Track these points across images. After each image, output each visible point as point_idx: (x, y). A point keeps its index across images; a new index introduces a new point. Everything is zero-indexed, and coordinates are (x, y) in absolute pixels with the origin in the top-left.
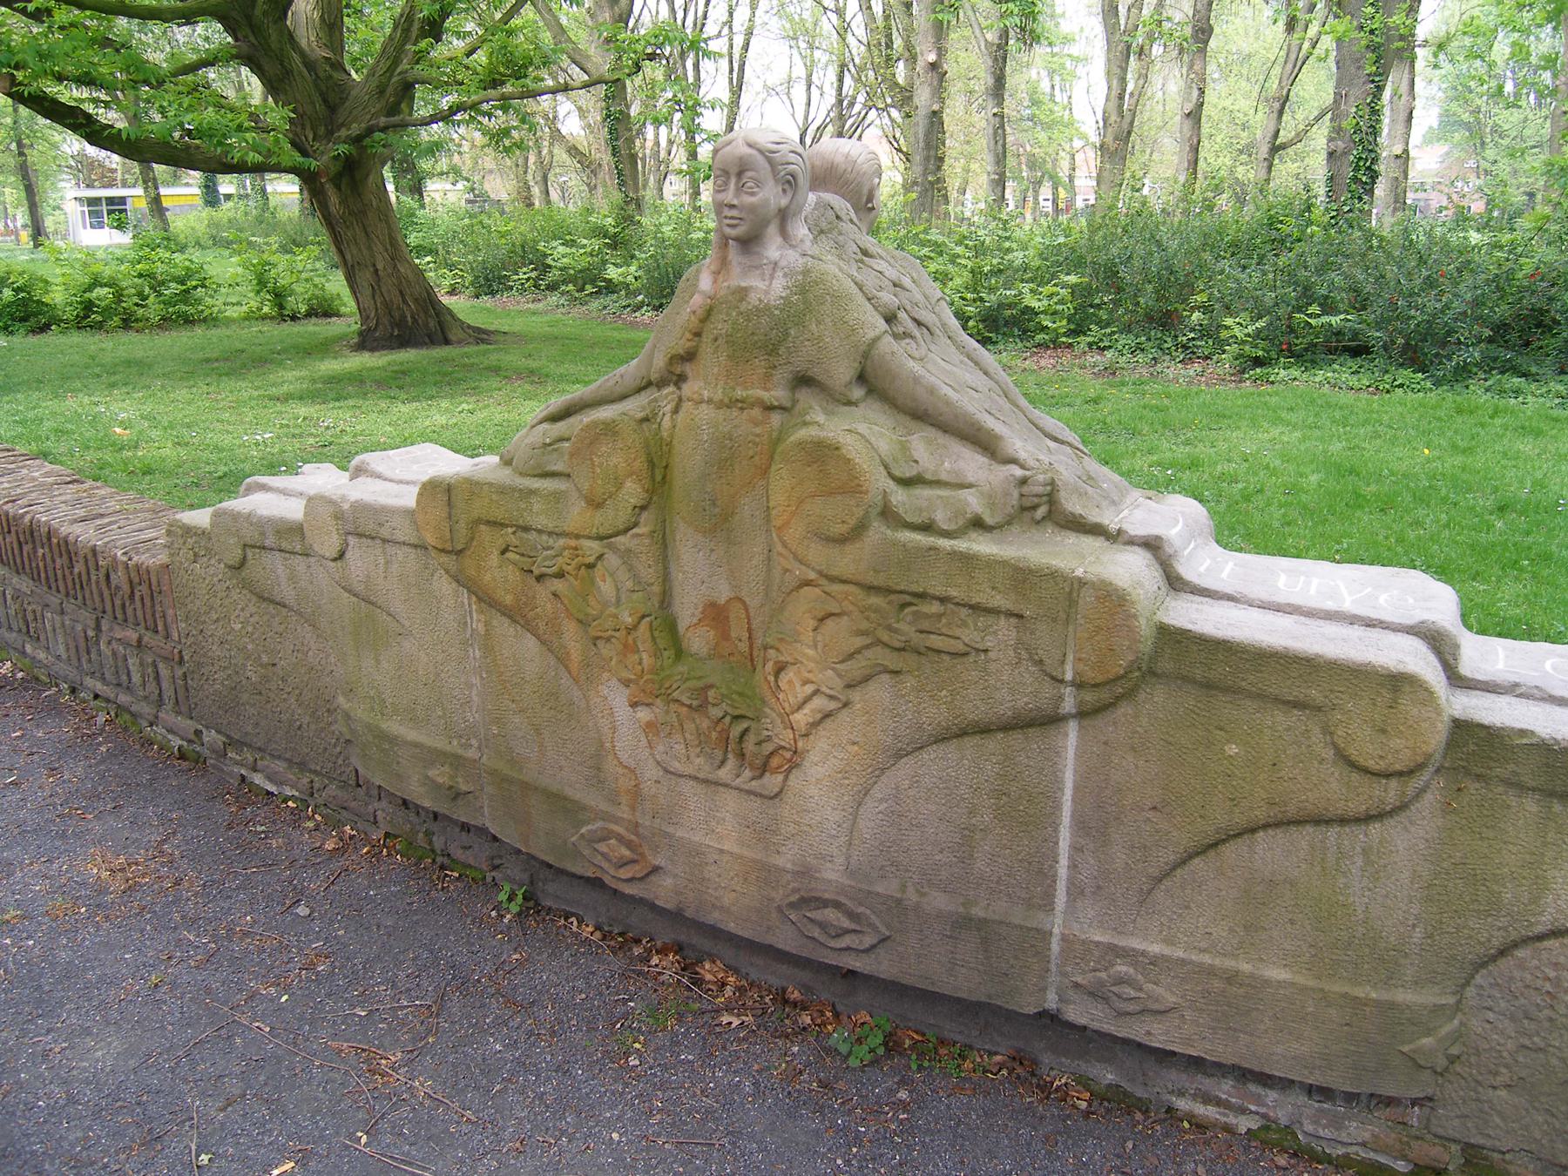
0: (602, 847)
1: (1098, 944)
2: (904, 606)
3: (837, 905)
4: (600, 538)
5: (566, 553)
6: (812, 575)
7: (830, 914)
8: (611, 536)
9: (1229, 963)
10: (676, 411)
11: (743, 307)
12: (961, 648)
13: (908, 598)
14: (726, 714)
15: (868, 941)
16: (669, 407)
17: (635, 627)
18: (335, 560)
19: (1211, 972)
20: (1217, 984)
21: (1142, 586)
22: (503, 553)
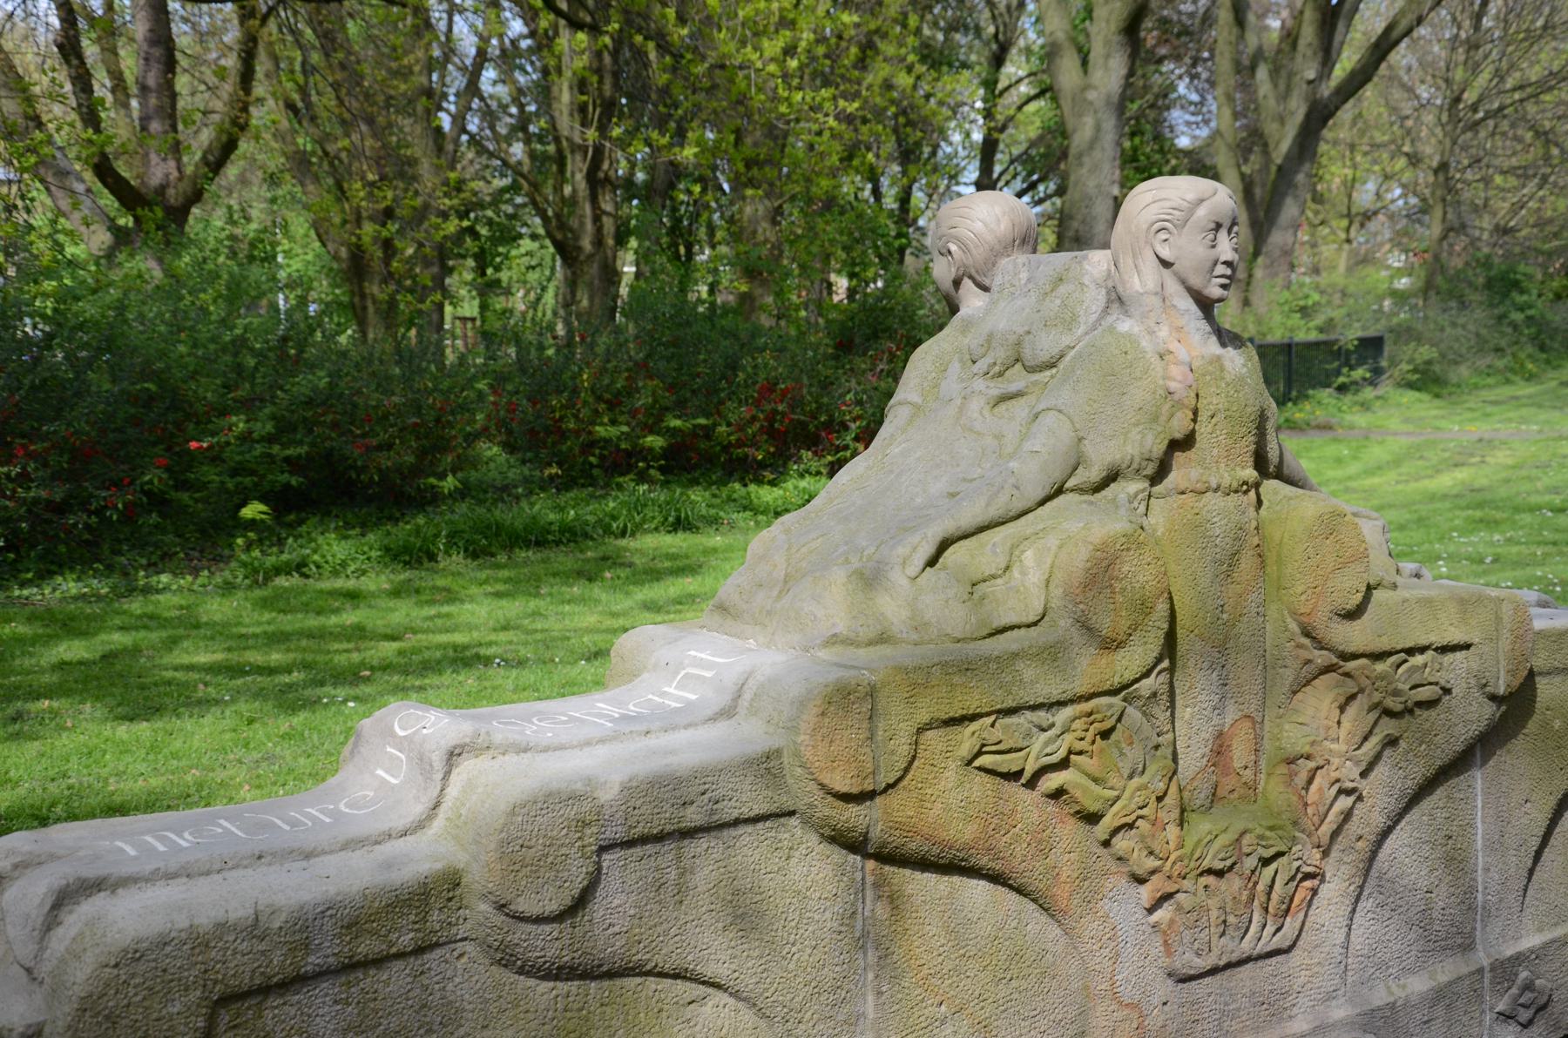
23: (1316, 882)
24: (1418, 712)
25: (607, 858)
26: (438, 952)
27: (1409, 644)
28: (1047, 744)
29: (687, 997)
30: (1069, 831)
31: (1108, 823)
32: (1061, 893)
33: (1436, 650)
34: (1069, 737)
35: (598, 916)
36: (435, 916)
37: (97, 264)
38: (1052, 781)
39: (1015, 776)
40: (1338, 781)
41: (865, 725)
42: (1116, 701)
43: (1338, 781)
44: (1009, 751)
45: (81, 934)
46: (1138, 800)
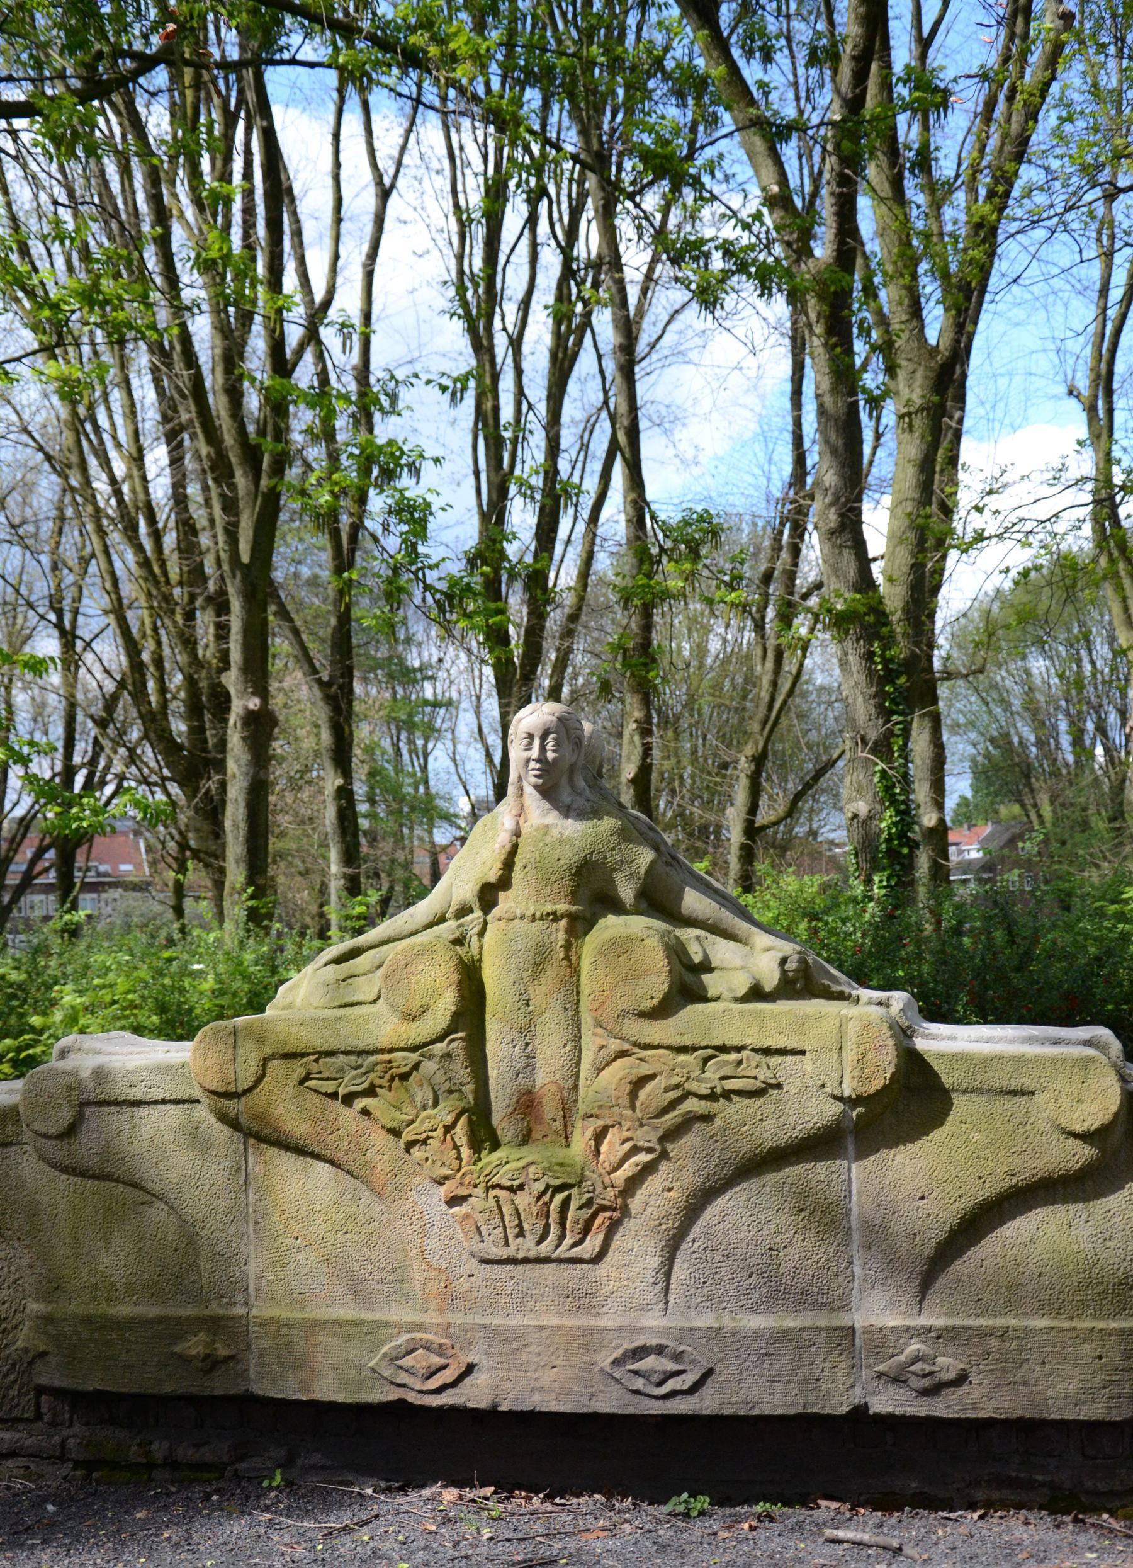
0: (407, 1362)
1: (893, 1329)
2: (706, 1060)
3: (660, 1350)
4: (414, 1049)
5: (379, 1067)
6: (627, 1047)
7: (649, 1362)
8: (426, 1044)
9: (1000, 1322)
10: (481, 934)
11: (548, 839)
12: (759, 1084)
13: (710, 1052)
14: (548, 1186)
15: (689, 1379)
16: (476, 930)
17: (453, 1125)
18: (60, 1137)
19: (987, 1333)
20: (995, 1342)
21: (402, 109)
22: (302, 1082)
23: (617, 1215)
24: (735, 1098)
25: (88, 1111)
26: (14, 1148)
27: (719, 1042)
28: (354, 1078)
29: (140, 1200)
30: (381, 1139)
31: (407, 1136)
32: (378, 1181)
33: (753, 1050)
34: (372, 1076)
35: (84, 1142)
36: (9, 1128)
37: (904, 802)
38: (360, 1103)
39: (334, 1095)
40: (631, 1139)
41: (230, 1051)
42: (414, 1057)
43: (631, 1139)
44: (327, 1079)
45: (946, 1314)
46: (427, 1125)
